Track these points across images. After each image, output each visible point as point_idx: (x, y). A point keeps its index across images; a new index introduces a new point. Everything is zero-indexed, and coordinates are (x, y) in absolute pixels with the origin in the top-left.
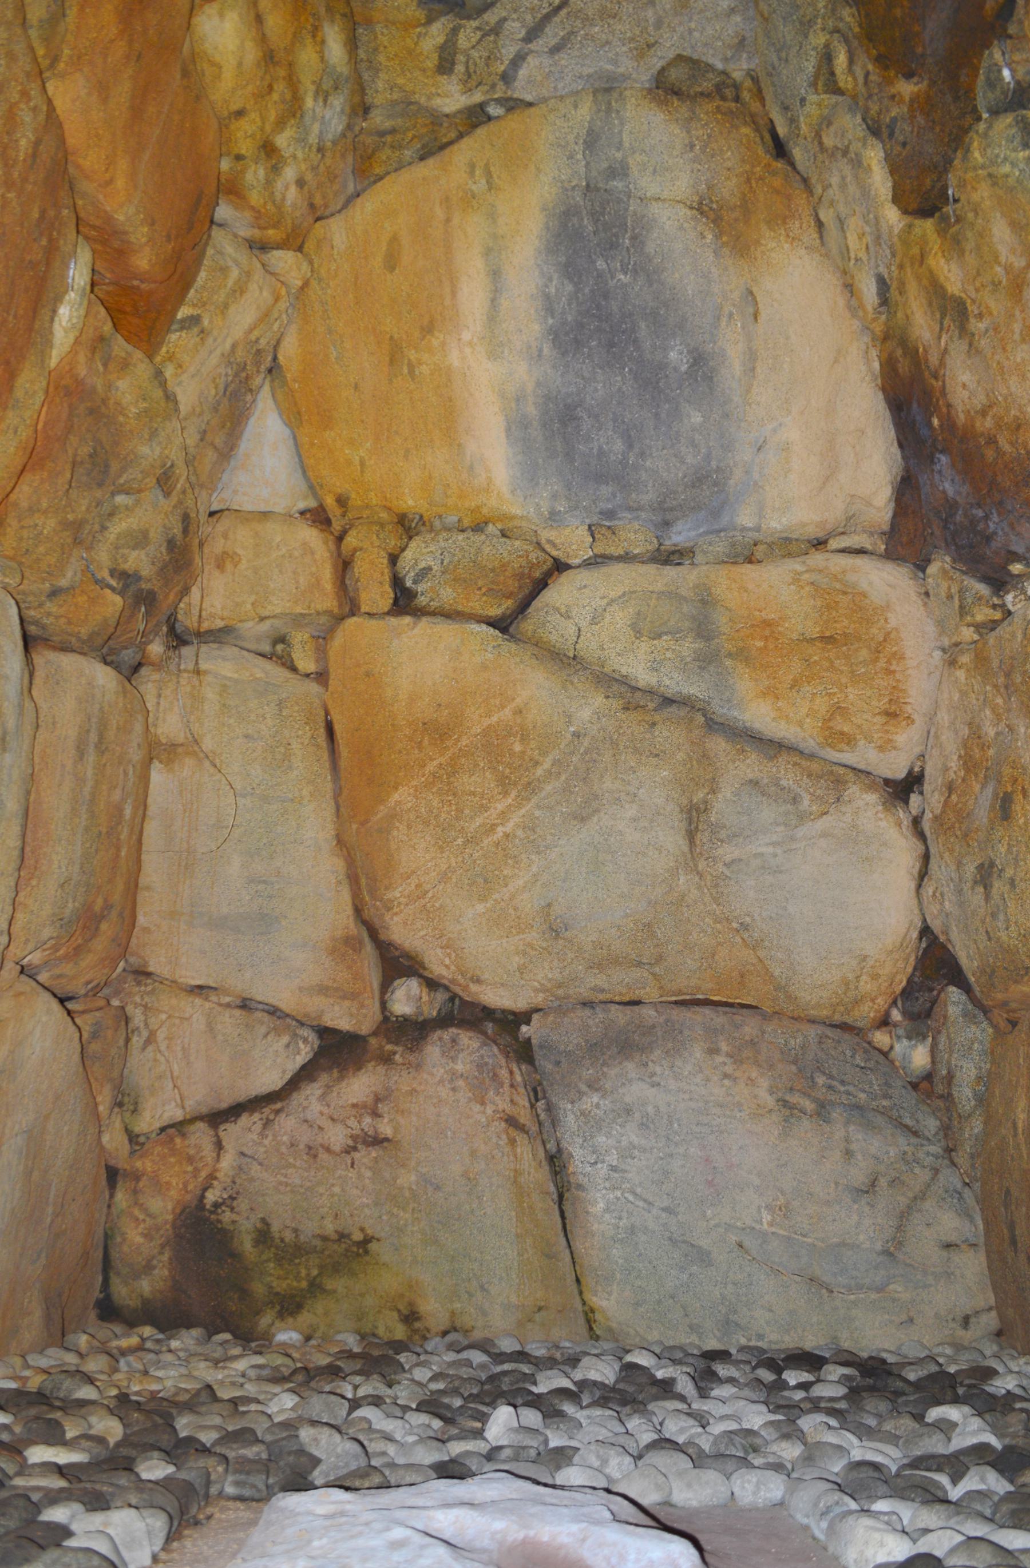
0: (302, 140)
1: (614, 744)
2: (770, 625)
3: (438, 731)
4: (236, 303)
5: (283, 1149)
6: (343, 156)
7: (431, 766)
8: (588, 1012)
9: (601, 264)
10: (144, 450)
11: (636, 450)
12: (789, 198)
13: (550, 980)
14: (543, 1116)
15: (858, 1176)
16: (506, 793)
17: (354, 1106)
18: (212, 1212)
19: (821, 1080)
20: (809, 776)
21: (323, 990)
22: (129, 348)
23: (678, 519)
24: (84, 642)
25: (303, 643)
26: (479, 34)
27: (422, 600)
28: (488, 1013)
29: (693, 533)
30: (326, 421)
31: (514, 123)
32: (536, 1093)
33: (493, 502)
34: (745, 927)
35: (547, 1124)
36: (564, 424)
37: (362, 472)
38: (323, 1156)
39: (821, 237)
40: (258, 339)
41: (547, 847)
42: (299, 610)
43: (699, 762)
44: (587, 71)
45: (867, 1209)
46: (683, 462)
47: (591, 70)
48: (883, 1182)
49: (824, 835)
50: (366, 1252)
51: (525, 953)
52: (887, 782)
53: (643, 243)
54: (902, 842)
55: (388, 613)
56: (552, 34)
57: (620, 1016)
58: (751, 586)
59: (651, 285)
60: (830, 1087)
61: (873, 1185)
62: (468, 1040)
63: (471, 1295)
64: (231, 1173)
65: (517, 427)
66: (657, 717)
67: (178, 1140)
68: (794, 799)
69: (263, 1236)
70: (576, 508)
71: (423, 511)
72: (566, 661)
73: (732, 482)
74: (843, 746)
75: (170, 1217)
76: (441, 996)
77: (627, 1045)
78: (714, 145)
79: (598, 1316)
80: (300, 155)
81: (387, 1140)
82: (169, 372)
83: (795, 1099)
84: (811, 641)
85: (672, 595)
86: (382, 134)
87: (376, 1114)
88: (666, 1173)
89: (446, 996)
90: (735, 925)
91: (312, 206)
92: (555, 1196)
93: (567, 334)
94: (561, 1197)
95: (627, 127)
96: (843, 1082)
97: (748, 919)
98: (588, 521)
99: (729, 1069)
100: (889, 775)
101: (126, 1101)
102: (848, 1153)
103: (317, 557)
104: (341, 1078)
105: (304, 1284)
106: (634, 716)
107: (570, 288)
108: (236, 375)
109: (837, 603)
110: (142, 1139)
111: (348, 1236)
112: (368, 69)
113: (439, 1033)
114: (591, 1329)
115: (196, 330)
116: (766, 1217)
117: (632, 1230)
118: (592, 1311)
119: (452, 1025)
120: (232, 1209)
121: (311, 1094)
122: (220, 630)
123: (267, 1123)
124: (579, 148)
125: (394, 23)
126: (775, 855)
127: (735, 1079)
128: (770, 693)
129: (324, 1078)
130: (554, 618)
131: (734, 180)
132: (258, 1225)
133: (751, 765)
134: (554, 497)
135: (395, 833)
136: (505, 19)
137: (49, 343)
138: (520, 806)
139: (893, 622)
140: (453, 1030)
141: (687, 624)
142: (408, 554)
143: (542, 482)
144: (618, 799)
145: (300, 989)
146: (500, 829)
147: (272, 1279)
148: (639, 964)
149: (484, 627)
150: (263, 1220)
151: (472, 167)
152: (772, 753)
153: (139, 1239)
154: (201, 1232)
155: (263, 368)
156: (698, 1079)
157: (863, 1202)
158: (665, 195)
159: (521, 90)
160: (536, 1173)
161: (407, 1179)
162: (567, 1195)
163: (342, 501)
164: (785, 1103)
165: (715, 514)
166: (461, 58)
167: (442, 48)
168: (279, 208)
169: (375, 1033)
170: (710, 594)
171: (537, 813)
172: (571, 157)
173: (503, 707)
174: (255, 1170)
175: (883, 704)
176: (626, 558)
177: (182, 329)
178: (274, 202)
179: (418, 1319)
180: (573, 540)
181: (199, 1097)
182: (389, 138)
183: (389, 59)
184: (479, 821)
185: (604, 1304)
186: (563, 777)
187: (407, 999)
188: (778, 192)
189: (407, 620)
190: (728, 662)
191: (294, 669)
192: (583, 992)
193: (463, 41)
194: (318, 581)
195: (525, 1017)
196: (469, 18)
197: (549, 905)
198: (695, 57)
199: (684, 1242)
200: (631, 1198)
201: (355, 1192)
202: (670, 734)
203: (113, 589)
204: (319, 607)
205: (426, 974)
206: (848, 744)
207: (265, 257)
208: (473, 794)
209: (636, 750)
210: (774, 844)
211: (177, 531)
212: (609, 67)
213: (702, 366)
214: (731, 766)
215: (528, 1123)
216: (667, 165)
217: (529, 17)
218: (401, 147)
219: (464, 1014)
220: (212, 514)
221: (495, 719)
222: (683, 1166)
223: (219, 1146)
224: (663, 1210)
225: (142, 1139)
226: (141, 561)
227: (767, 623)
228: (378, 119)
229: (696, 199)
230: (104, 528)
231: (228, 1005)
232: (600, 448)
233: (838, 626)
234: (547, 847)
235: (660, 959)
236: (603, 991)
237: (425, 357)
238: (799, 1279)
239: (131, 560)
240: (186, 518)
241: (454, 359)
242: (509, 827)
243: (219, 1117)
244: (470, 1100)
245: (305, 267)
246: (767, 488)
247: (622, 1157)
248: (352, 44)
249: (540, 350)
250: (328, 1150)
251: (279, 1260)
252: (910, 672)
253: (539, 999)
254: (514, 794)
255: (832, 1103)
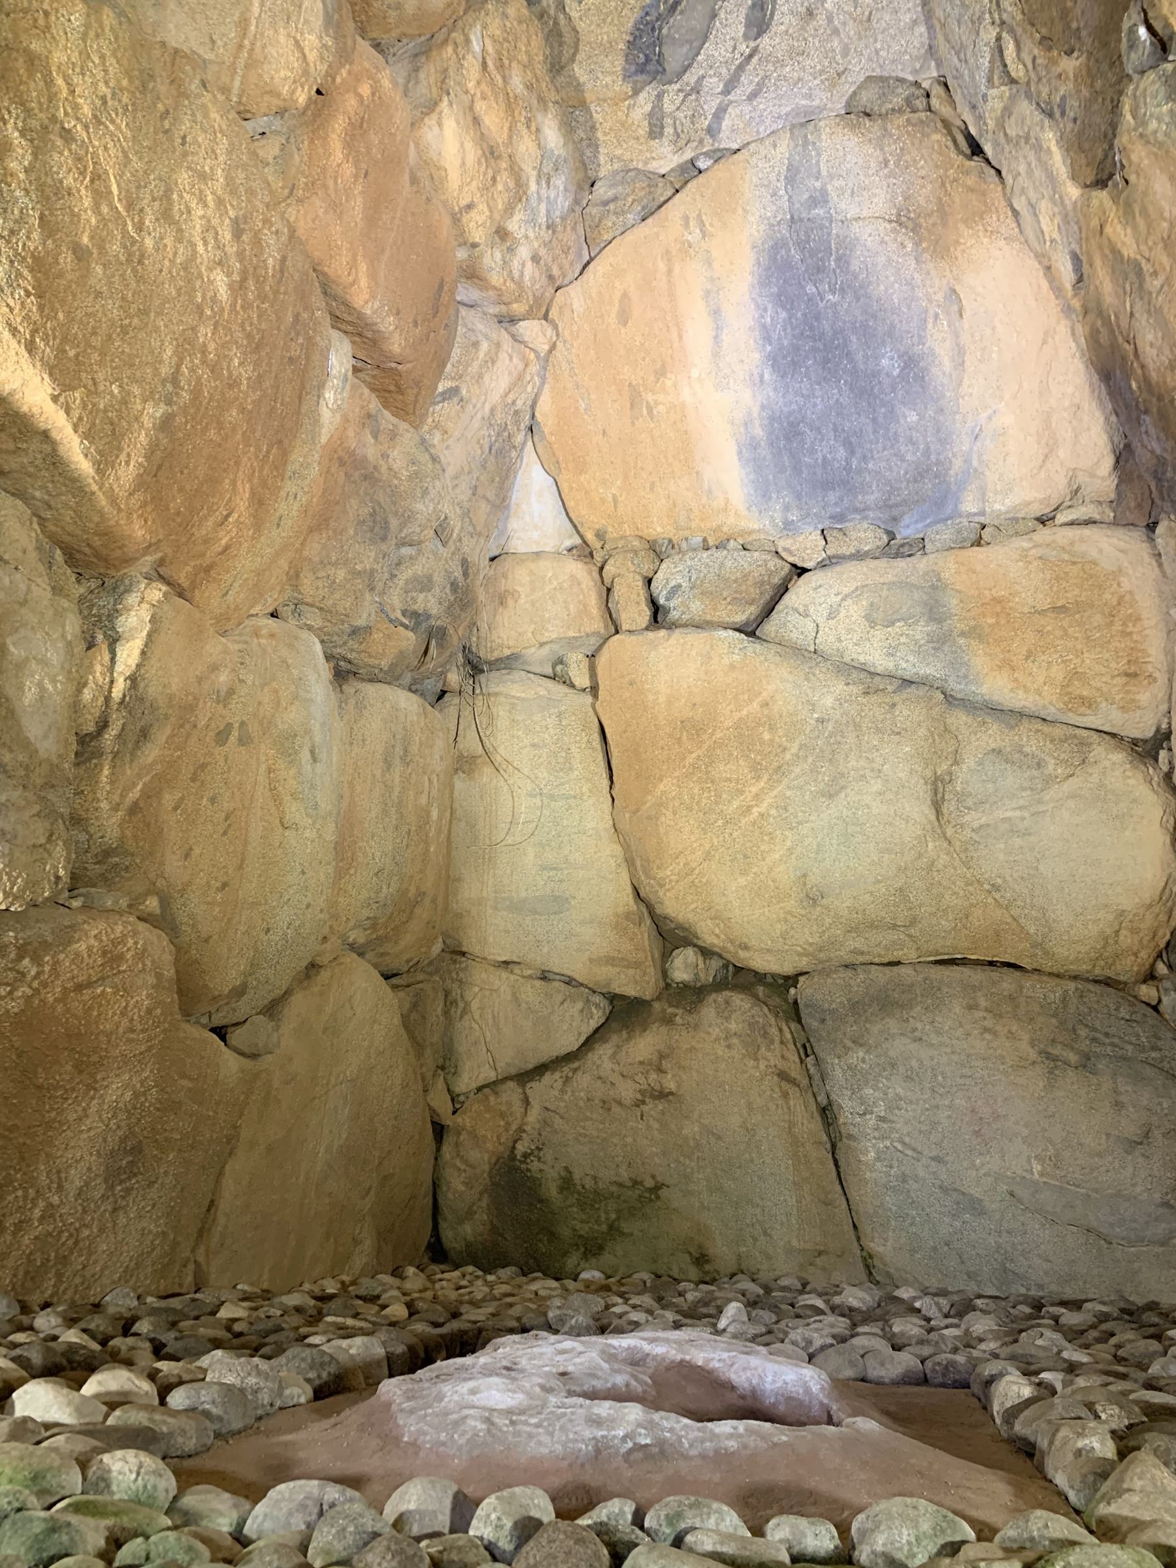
0: (532, 221)
1: (857, 726)
2: (1000, 602)
3: (693, 729)
4: (490, 375)
5: (582, 1104)
6: (574, 229)
7: (691, 759)
8: (850, 973)
9: (810, 289)
10: (419, 506)
11: (858, 455)
12: (984, 194)
13: (811, 944)
14: (812, 1070)
15: (1129, 1128)
16: (758, 778)
17: (641, 1063)
18: (524, 1162)
19: (1083, 1032)
20: (1052, 741)
21: (610, 961)
22: (395, 420)
23: (904, 513)
24: (386, 673)
25: (579, 662)
26: (681, 95)
27: (674, 615)
28: (760, 977)
29: (920, 525)
30: (581, 467)
31: (720, 172)
32: (806, 1050)
33: (731, 520)
34: (996, 888)
35: (817, 1077)
36: (788, 439)
37: (615, 507)
38: (616, 1109)
39: (1019, 225)
40: (514, 403)
41: (799, 823)
42: (571, 634)
43: (940, 735)
44: (785, 110)
45: (1141, 1160)
46: (903, 460)
47: (789, 109)
48: (1157, 1133)
49: (1072, 796)
50: (658, 1198)
51: (786, 921)
52: (1135, 742)
53: (848, 263)
54: (1152, 797)
55: (647, 629)
56: (747, 83)
57: (882, 976)
58: (979, 568)
59: (858, 300)
60: (1094, 1040)
61: (1147, 1136)
62: (740, 1001)
63: (755, 1240)
64: (537, 1126)
65: (749, 450)
66: (897, 699)
67: (492, 1098)
68: (1039, 764)
69: (567, 1183)
70: (808, 515)
71: (671, 536)
72: (809, 655)
73: (952, 472)
74: (1083, 709)
75: (487, 1168)
76: (715, 964)
77: (887, 1003)
78: (907, 157)
79: (876, 1262)
80: (531, 235)
81: (671, 1093)
82: (437, 438)
83: (1056, 1051)
84: (1042, 613)
85: (902, 585)
86: (606, 203)
87: (660, 1070)
88: (934, 1124)
89: (721, 963)
90: (986, 887)
91: (551, 277)
92: (828, 1146)
93: (784, 357)
94: (834, 1146)
95: (824, 157)
96: (1107, 1035)
97: (999, 881)
98: (821, 527)
99: (988, 1023)
100: (1137, 734)
101: (447, 1064)
102: (1118, 1105)
103: (584, 586)
104: (629, 1039)
105: (604, 1228)
106: (874, 698)
107: (783, 315)
108: (499, 435)
109: (1066, 573)
110: (462, 1098)
111: (641, 1183)
112: (589, 146)
113: (714, 995)
114: (871, 1273)
115: (456, 399)
116: (1037, 1167)
117: (904, 1178)
118: (871, 1257)
119: (727, 989)
120: (539, 1159)
121: (602, 1054)
122: (508, 657)
123: (567, 1080)
124: (781, 184)
125: (605, 100)
126: (1023, 819)
127: (995, 1034)
128: (1007, 665)
129: (615, 1039)
130: (793, 618)
131: (929, 187)
132: (563, 1174)
133: (994, 735)
134: (787, 508)
135: (663, 819)
136: (704, 77)
137: (316, 422)
138: (772, 788)
139: (1126, 585)
140: (727, 993)
141: (918, 609)
142: (660, 575)
143: (774, 496)
144: (864, 776)
145: (591, 960)
146: (755, 810)
147: (574, 1223)
148: (895, 927)
149: (731, 632)
150: (566, 1168)
151: (686, 219)
152: (1013, 722)
153: (462, 1188)
154: (513, 1180)
155: (522, 426)
156: (959, 1032)
157: (1137, 1153)
158: (865, 214)
159: (727, 141)
160: (810, 1126)
161: (691, 1129)
162: (839, 1145)
163: (600, 535)
164: (1049, 1056)
165: (940, 503)
166: (668, 121)
167: (650, 115)
168: (520, 284)
169: (658, 998)
170: (939, 580)
171: (788, 793)
172: (774, 195)
173: (751, 700)
174: (558, 1122)
175: (1122, 665)
176: (859, 556)
177: (443, 400)
178: (513, 280)
179: (708, 1262)
180: (806, 546)
181: (509, 1060)
182: (612, 206)
183: (605, 134)
184: (735, 804)
185: (881, 1249)
186: (810, 760)
187: (684, 966)
188: (972, 190)
189: (662, 633)
190: (962, 641)
191: (573, 686)
192: (843, 954)
193: (668, 107)
194: (585, 606)
195: (792, 980)
196: (670, 82)
197: (805, 876)
198: (885, 74)
199: (955, 1190)
200: (900, 1147)
201: (645, 1142)
202: (910, 712)
203: (406, 627)
204: (588, 630)
205: (700, 943)
206: (1090, 707)
207: (513, 329)
208: (730, 780)
209: (878, 730)
210: (1021, 808)
211: (458, 573)
212: (804, 102)
213: (914, 368)
214: (973, 738)
215: (798, 1077)
216: (863, 185)
217: (724, 71)
218: (623, 212)
219: (738, 977)
220: (492, 559)
221: (745, 712)
222: (949, 1117)
223: (526, 1102)
224: (933, 1159)
225: (462, 1098)
226: (431, 603)
227: (997, 601)
228: (602, 191)
229: (894, 212)
230: (393, 576)
231: (530, 977)
232: (824, 458)
233: (1069, 595)
234: (799, 823)
235: (913, 922)
236: (862, 953)
237: (661, 398)
238: (1075, 1229)
239: (420, 600)
240: (465, 563)
241: (686, 395)
242: (763, 807)
243: (526, 1077)
244: (744, 1056)
245: (550, 331)
246: (987, 473)
247: (890, 1109)
248: (568, 127)
249: (762, 376)
250: (620, 1103)
251: (582, 1205)
252: (1148, 632)
253: (803, 964)
254: (766, 777)
255: (1098, 1056)
